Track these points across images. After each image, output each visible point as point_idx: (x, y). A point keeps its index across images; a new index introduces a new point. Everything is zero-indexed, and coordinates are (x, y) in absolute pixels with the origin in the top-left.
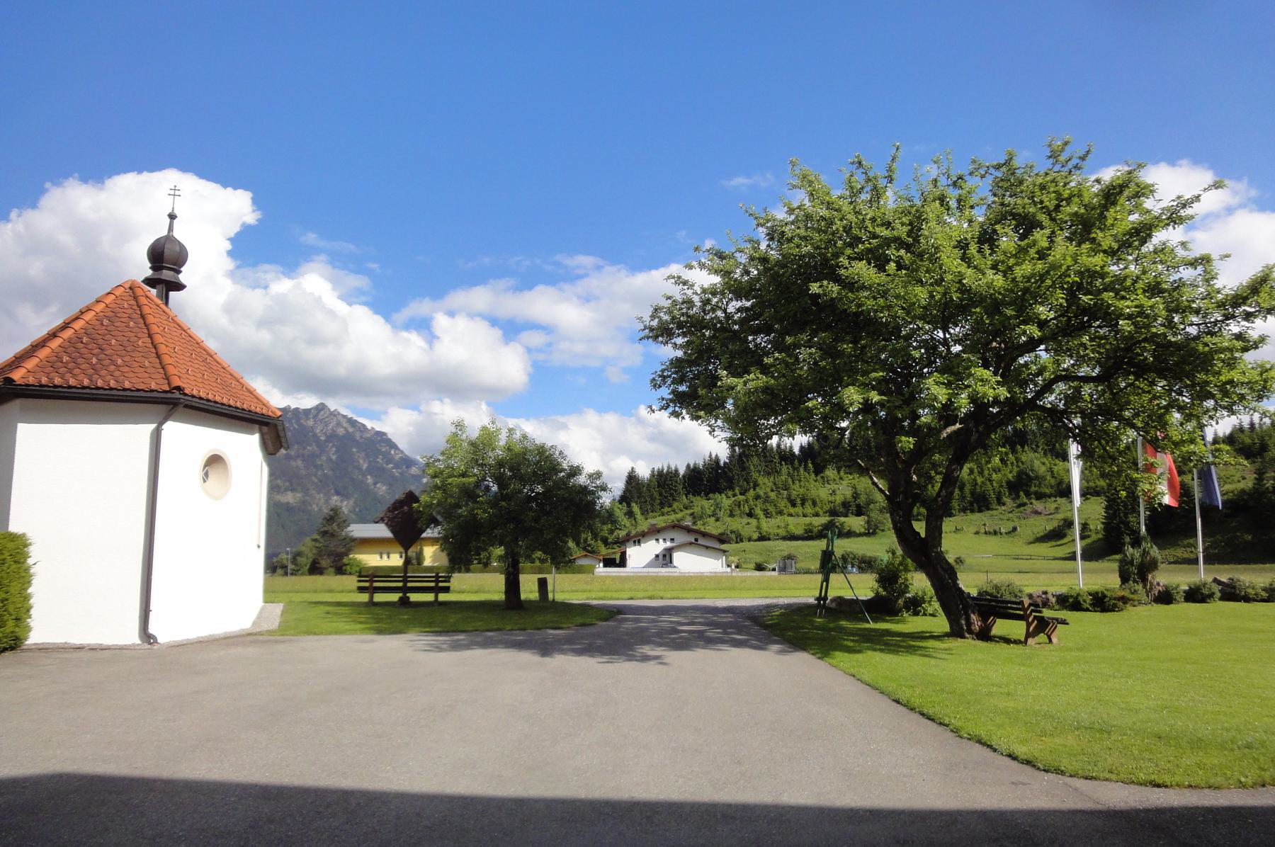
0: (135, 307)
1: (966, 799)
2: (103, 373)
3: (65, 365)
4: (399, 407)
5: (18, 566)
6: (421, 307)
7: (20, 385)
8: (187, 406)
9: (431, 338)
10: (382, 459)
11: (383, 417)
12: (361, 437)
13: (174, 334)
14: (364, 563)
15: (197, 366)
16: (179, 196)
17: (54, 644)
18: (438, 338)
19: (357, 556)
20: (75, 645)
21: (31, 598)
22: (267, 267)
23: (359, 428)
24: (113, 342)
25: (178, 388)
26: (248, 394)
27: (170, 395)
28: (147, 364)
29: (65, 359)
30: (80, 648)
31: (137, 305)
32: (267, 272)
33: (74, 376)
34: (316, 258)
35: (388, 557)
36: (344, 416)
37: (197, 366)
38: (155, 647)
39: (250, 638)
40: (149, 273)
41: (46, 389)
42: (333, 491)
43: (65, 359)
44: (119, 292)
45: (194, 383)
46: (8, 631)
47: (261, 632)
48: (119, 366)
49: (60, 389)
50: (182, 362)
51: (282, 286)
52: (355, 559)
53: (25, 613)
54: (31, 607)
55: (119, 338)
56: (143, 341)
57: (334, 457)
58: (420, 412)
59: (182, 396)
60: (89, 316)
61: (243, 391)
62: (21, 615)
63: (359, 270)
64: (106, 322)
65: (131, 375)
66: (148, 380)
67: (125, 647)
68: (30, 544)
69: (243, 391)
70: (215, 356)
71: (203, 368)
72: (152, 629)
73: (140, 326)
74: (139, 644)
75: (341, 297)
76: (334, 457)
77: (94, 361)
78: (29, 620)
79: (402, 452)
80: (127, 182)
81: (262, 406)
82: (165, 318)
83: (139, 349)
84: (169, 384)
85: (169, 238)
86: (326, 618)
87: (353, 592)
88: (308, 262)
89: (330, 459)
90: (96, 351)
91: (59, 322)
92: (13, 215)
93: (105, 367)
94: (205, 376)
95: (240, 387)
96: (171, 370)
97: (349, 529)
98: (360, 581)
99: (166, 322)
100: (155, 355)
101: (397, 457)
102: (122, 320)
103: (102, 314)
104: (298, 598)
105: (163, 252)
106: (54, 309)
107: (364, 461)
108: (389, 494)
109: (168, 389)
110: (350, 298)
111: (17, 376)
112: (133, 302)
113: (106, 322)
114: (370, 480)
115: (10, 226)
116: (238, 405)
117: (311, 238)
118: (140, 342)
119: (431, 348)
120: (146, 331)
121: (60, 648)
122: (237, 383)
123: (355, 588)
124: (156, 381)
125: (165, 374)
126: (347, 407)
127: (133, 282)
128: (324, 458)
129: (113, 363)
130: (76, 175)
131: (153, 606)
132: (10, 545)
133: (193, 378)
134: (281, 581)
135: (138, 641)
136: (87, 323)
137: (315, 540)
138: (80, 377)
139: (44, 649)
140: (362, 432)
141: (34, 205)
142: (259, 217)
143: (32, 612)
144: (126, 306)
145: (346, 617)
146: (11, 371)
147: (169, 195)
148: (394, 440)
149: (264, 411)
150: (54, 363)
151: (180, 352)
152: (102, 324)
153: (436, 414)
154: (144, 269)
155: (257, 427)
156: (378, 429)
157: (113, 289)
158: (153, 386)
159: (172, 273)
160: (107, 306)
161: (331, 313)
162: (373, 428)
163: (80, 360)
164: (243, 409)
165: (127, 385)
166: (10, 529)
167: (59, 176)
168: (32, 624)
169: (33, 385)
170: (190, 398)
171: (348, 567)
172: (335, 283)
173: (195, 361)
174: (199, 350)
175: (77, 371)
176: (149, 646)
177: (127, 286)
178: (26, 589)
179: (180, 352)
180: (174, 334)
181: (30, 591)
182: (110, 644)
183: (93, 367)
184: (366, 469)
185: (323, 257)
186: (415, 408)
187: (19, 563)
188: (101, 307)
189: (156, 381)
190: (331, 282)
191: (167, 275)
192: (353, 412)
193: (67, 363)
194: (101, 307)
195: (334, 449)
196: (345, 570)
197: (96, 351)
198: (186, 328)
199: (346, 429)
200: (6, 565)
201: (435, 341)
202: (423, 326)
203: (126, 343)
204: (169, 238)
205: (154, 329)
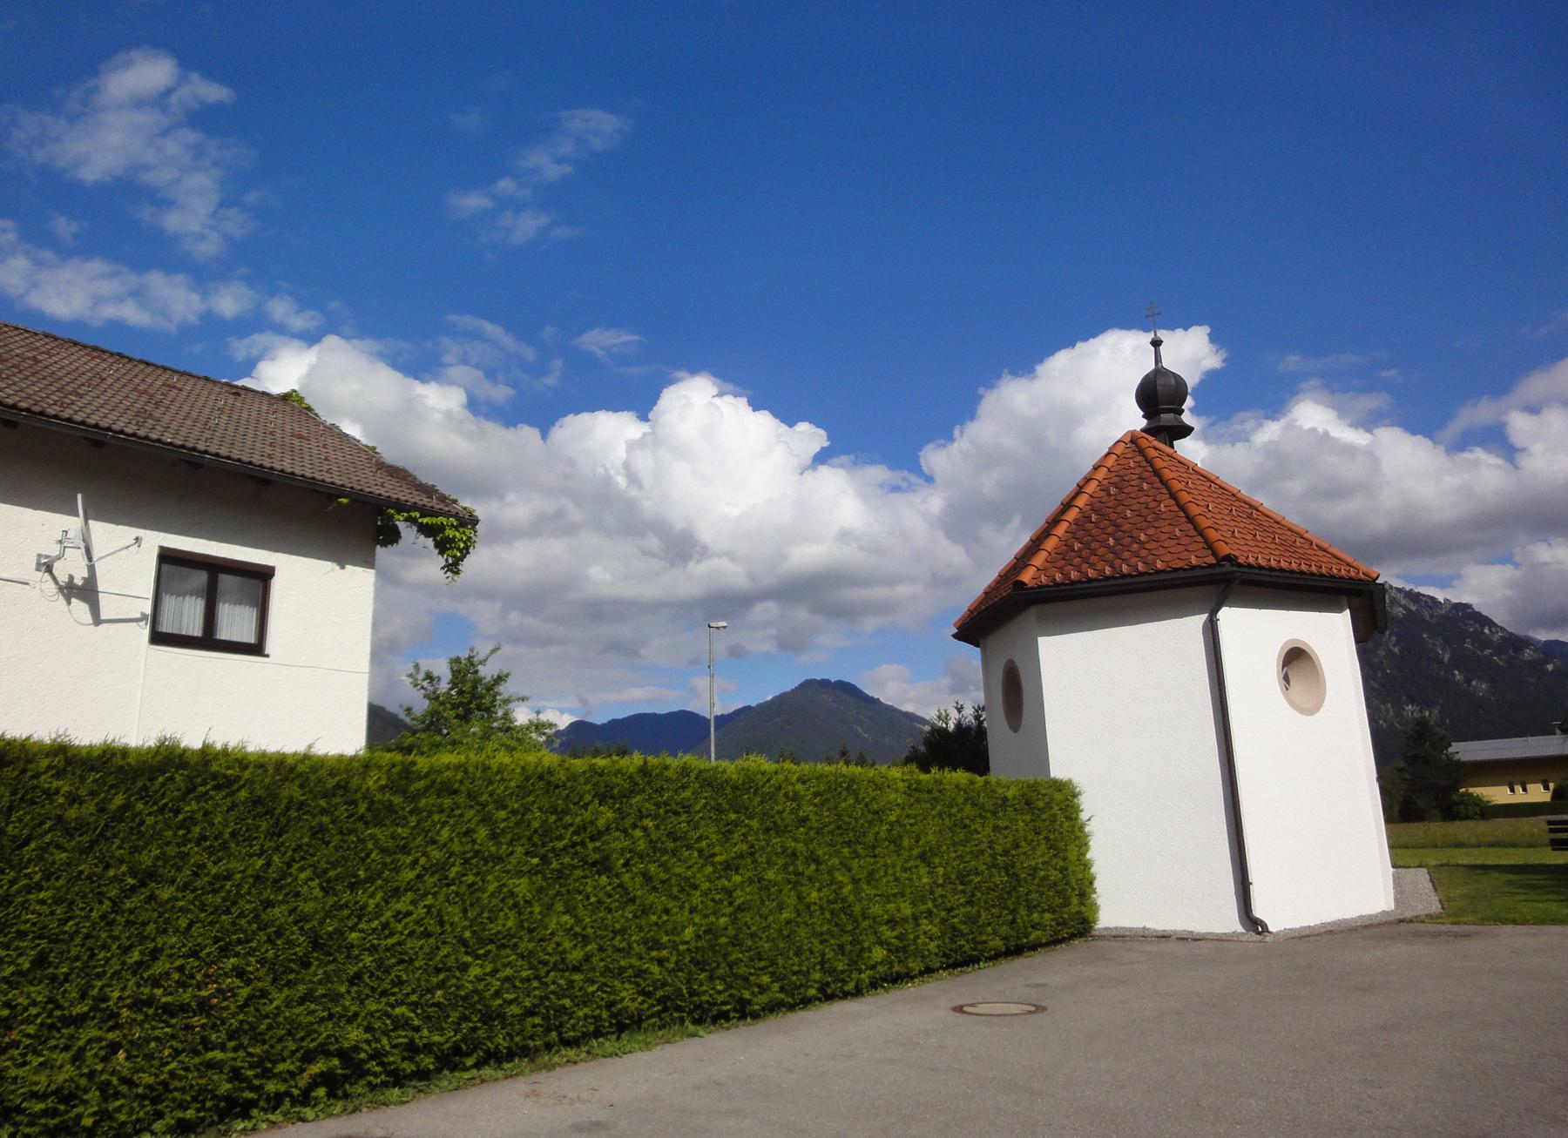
0: (1144, 464)
1: (1008, 889)
2: (1126, 555)
3: (1079, 554)
4: (1478, 564)
5: (1071, 823)
6: (1481, 413)
7: (1032, 588)
8: (1245, 582)
9: (1510, 452)
10: (1472, 645)
11: (1456, 583)
12: (1432, 616)
13: (1201, 488)
14: (1485, 799)
15: (1242, 525)
16: (1160, 314)
17: (1130, 929)
18: (1523, 450)
19: (1471, 790)
20: (1157, 931)
21: (1092, 865)
22: (1242, 415)
23: (1426, 603)
24: (1128, 513)
25: (1228, 558)
26: (1320, 553)
27: (1218, 570)
28: (1178, 533)
29: (1077, 546)
30: (1165, 937)
31: (1146, 460)
32: (1244, 420)
33: (1092, 566)
34: (1304, 385)
35: (1525, 790)
36: (1399, 590)
37: (1242, 525)
38: (1267, 939)
39: (1403, 927)
40: (1143, 423)
41: (1063, 587)
42: (1405, 698)
43: (1077, 546)
44: (1120, 449)
45: (1245, 548)
46: (1073, 910)
47: (1417, 917)
48: (1144, 543)
49: (1079, 586)
50: (1222, 522)
51: (1270, 432)
52: (1471, 795)
53: (1088, 887)
54: (1094, 879)
55: (1134, 508)
56: (1165, 505)
57: (1396, 650)
58: (1516, 565)
59: (1236, 569)
60: (1091, 488)
61: (1313, 549)
62: (1084, 888)
63: (1369, 389)
64: (1113, 490)
65: (1162, 551)
66: (1184, 555)
67: (1224, 937)
68: (1079, 794)
69: (1313, 549)
70: (1260, 508)
71: (1252, 527)
72: (1259, 911)
73: (1155, 486)
74: (1242, 934)
75: (1356, 425)
76: (1396, 650)
77: (1111, 542)
78: (1094, 896)
79: (1502, 628)
80: (1060, 362)
81: (1347, 568)
82: (1183, 470)
83: (1163, 516)
84: (1214, 554)
85: (1159, 372)
86: (1518, 893)
87: (1546, 845)
88: (1297, 393)
89: (1394, 654)
90: (1110, 529)
91: (1025, 539)
92: (956, 433)
93: (1127, 548)
94: (1258, 537)
95: (1307, 546)
96: (1213, 535)
97: (1451, 750)
98: (1551, 831)
99: (1185, 475)
100: (1185, 519)
101: (1495, 638)
102: (1133, 483)
103: (1106, 481)
104: (1463, 857)
105: (1156, 392)
106: (1016, 522)
107: (1444, 650)
108: (1494, 695)
109: (1215, 562)
110: (1368, 422)
111: (1027, 577)
112: (1140, 458)
113: (1113, 490)
114: (1458, 675)
115: (956, 444)
116: (1314, 569)
117: (1292, 361)
118: (1162, 506)
119: (1516, 467)
120: (1165, 491)
121: (1138, 936)
122: (1302, 541)
123: (1547, 841)
124: (1196, 553)
125: (1206, 543)
126: (1398, 576)
127: (1133, 433)
128: (1382, 653)
129: (1135, 540)
130: (1006, 371)
131: (1253, 876)
132: (1058, 796)
133: (1242, 542)
134: (1416, 830)
135: (1240, 929)
136: (1091, 496)
137: (1400, 770)
138: (1099, 566)
139: (1121, 937)
140: (1430, 608)
141: (972, 416)
142: (1225, 355)
143: (1096, 884)
144: (1132, 465)
145: (1554, 893)
146: (1019, 573)
147: (1146, 317)
148: (1484, 613)
149: (1353, 574)
150: (1064, 554)
151: (1216, 511)
152: (1109, 495)
153: (1547, 564)
154: (1136, 420)
155: (1344, 599)
156: (1455, 600)
157: (1110, 449)
158: (1194, 561)
159: (1171, 416)
160: (1109, 470)
161: (1349, 451)
162: (1446, 600)
163: (1094, 545)
164: (1322, 575)
165: (1159, 565)
166: (1052, 775)
167: (990, 379)
168: (1099, 902)
169: (1047, 586)
170: (1246, 570)
171: (1462, 808)
172: (1342, 412)
173: (1239, 519)
174: (1238, 504)
175: (1093, 559)
176: (1258, 937)
177: (1127, 440)
178: (1084, 854)
179: (1216, 511)
180: (1201, 488)
181: (1089, 856)
182: (1203, 931)
183: (1111, 550)
184: (1449, 661)
185: (1314, 382)
186: (1507, 560)
187: (1071, 819)
188: (1103, 472)
189: (1196, 553)
190: (1333, 408)
191: (1166, 418)
192: (1408, 581)
193: (1080, 550)
194: (1103, 472)
195: (1394, 639)
196: (1458, 812)
197: (1110, 529)
198: (1213, 478)
199: (1405, 607)
200: (1058, 822)
201: (1518, 455)
202: (1496, 439)
203: (1144, 512)
204: (1159, 372)
205: (1176, 485)
